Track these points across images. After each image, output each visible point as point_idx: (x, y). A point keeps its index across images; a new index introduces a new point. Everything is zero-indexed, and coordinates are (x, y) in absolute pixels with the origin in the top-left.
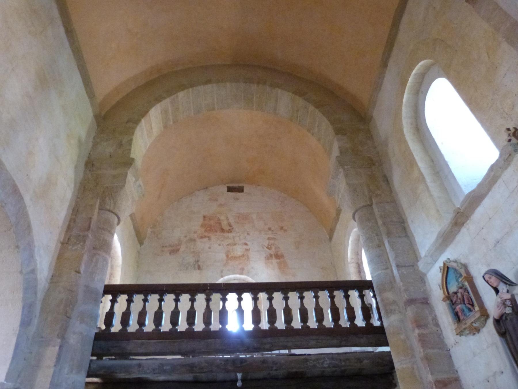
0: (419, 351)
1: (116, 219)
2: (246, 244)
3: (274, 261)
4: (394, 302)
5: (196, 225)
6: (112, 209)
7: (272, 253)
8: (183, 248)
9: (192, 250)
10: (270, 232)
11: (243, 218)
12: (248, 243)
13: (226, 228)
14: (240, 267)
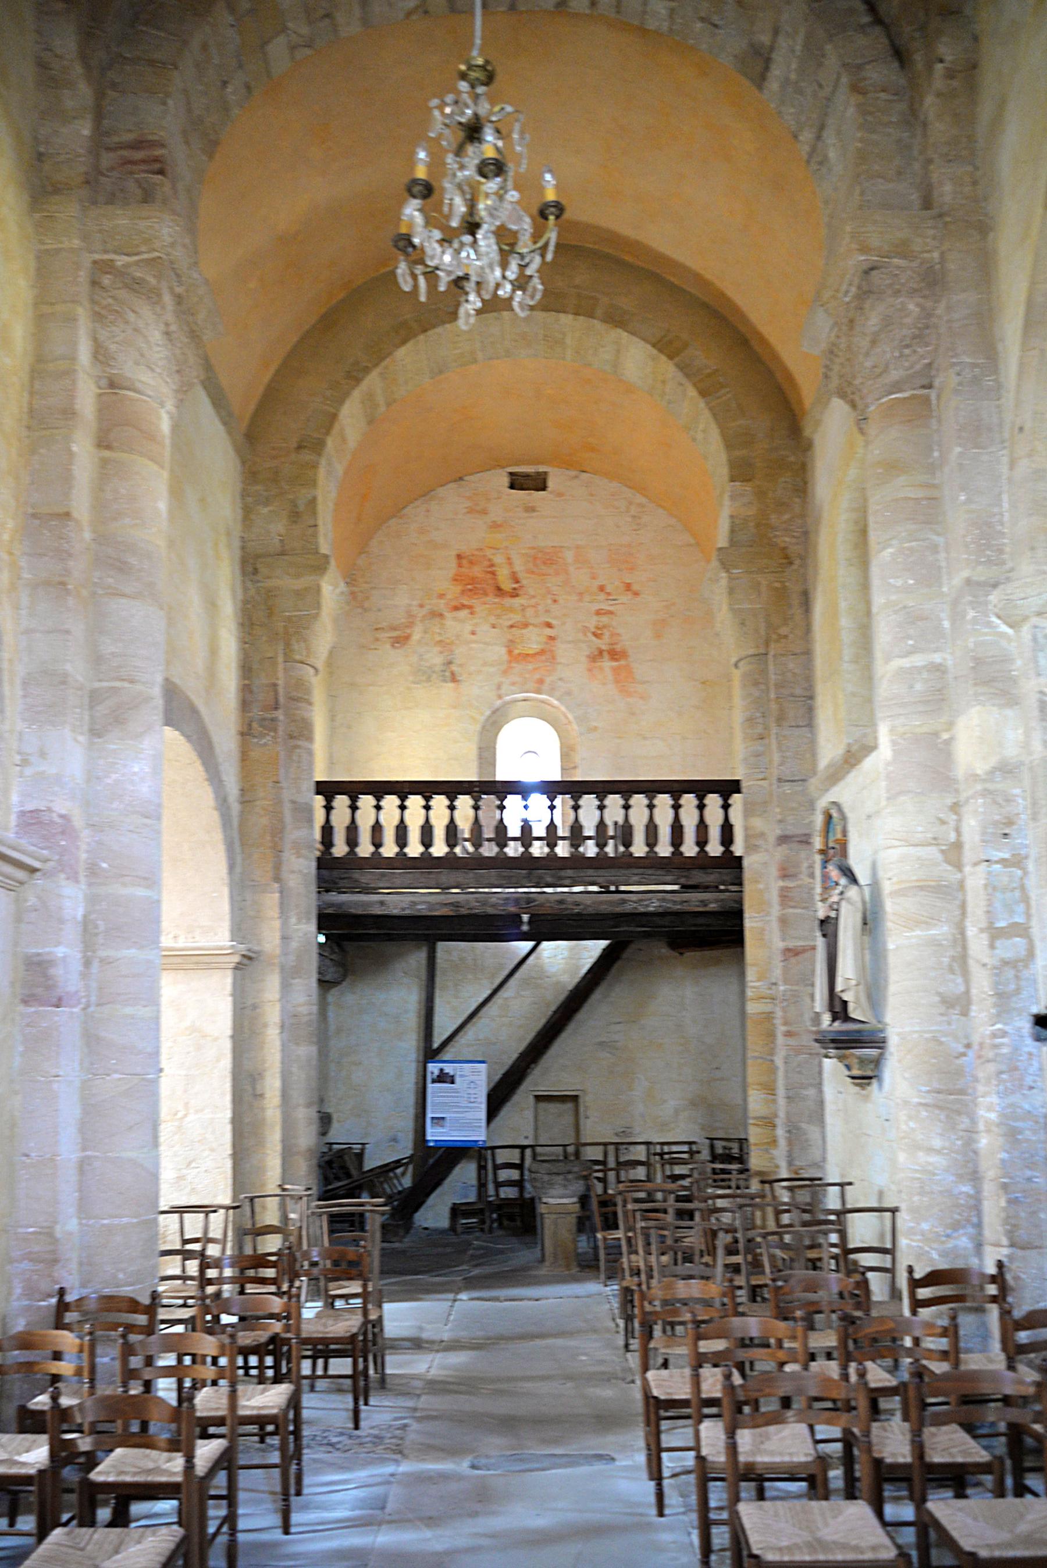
0: (776, 910)
1: (311, 671)
2: (549, 625)
3: (607, 664)
4: (762, 835)
5: (442, 577)
6: (303, 658)
7: (604, 647)
8: (417, 635)
9: (438, 638)
10: (602, 596)
11: (546, 560)
12: (553, 622)
13: (507, 585)
14: (537, 676)
